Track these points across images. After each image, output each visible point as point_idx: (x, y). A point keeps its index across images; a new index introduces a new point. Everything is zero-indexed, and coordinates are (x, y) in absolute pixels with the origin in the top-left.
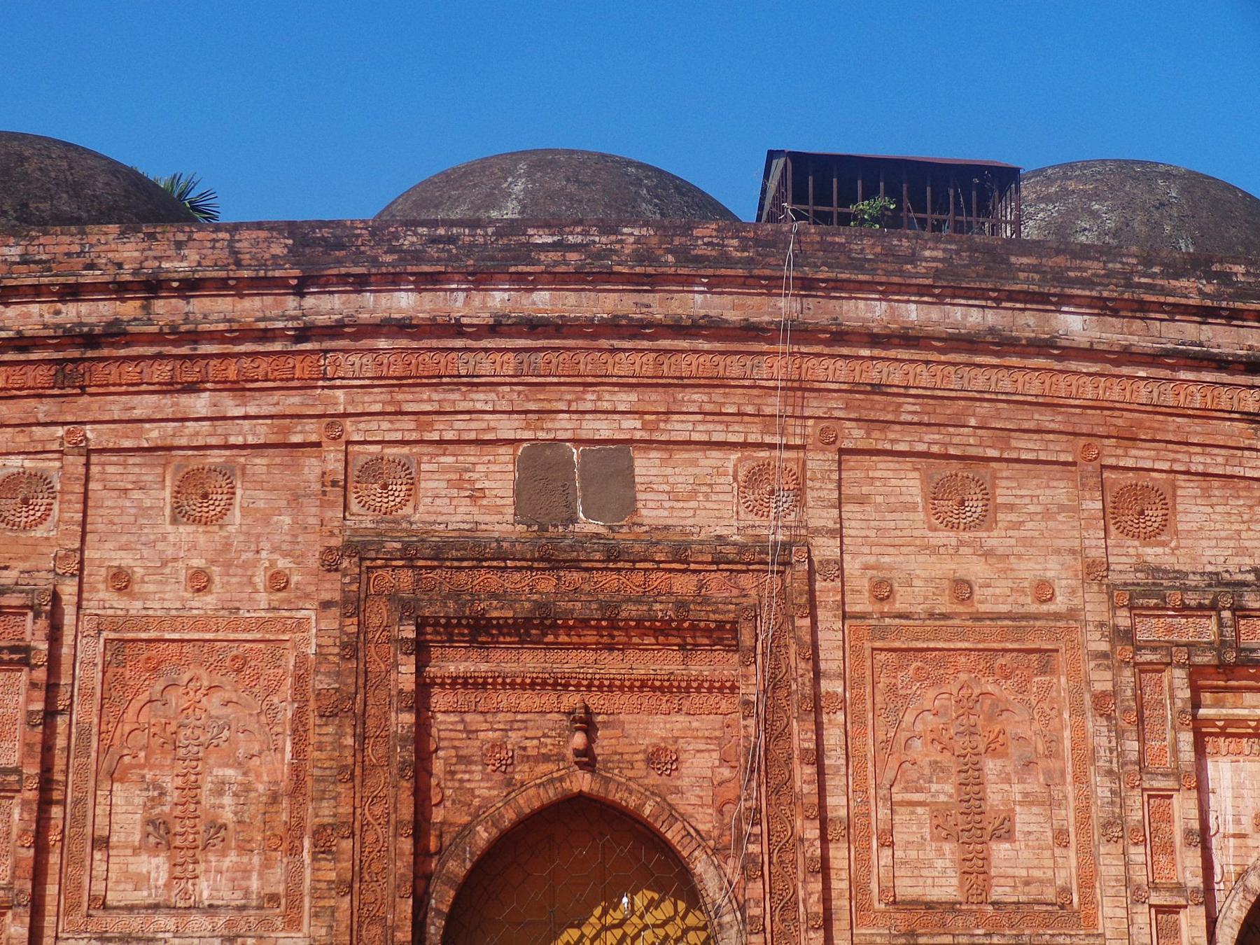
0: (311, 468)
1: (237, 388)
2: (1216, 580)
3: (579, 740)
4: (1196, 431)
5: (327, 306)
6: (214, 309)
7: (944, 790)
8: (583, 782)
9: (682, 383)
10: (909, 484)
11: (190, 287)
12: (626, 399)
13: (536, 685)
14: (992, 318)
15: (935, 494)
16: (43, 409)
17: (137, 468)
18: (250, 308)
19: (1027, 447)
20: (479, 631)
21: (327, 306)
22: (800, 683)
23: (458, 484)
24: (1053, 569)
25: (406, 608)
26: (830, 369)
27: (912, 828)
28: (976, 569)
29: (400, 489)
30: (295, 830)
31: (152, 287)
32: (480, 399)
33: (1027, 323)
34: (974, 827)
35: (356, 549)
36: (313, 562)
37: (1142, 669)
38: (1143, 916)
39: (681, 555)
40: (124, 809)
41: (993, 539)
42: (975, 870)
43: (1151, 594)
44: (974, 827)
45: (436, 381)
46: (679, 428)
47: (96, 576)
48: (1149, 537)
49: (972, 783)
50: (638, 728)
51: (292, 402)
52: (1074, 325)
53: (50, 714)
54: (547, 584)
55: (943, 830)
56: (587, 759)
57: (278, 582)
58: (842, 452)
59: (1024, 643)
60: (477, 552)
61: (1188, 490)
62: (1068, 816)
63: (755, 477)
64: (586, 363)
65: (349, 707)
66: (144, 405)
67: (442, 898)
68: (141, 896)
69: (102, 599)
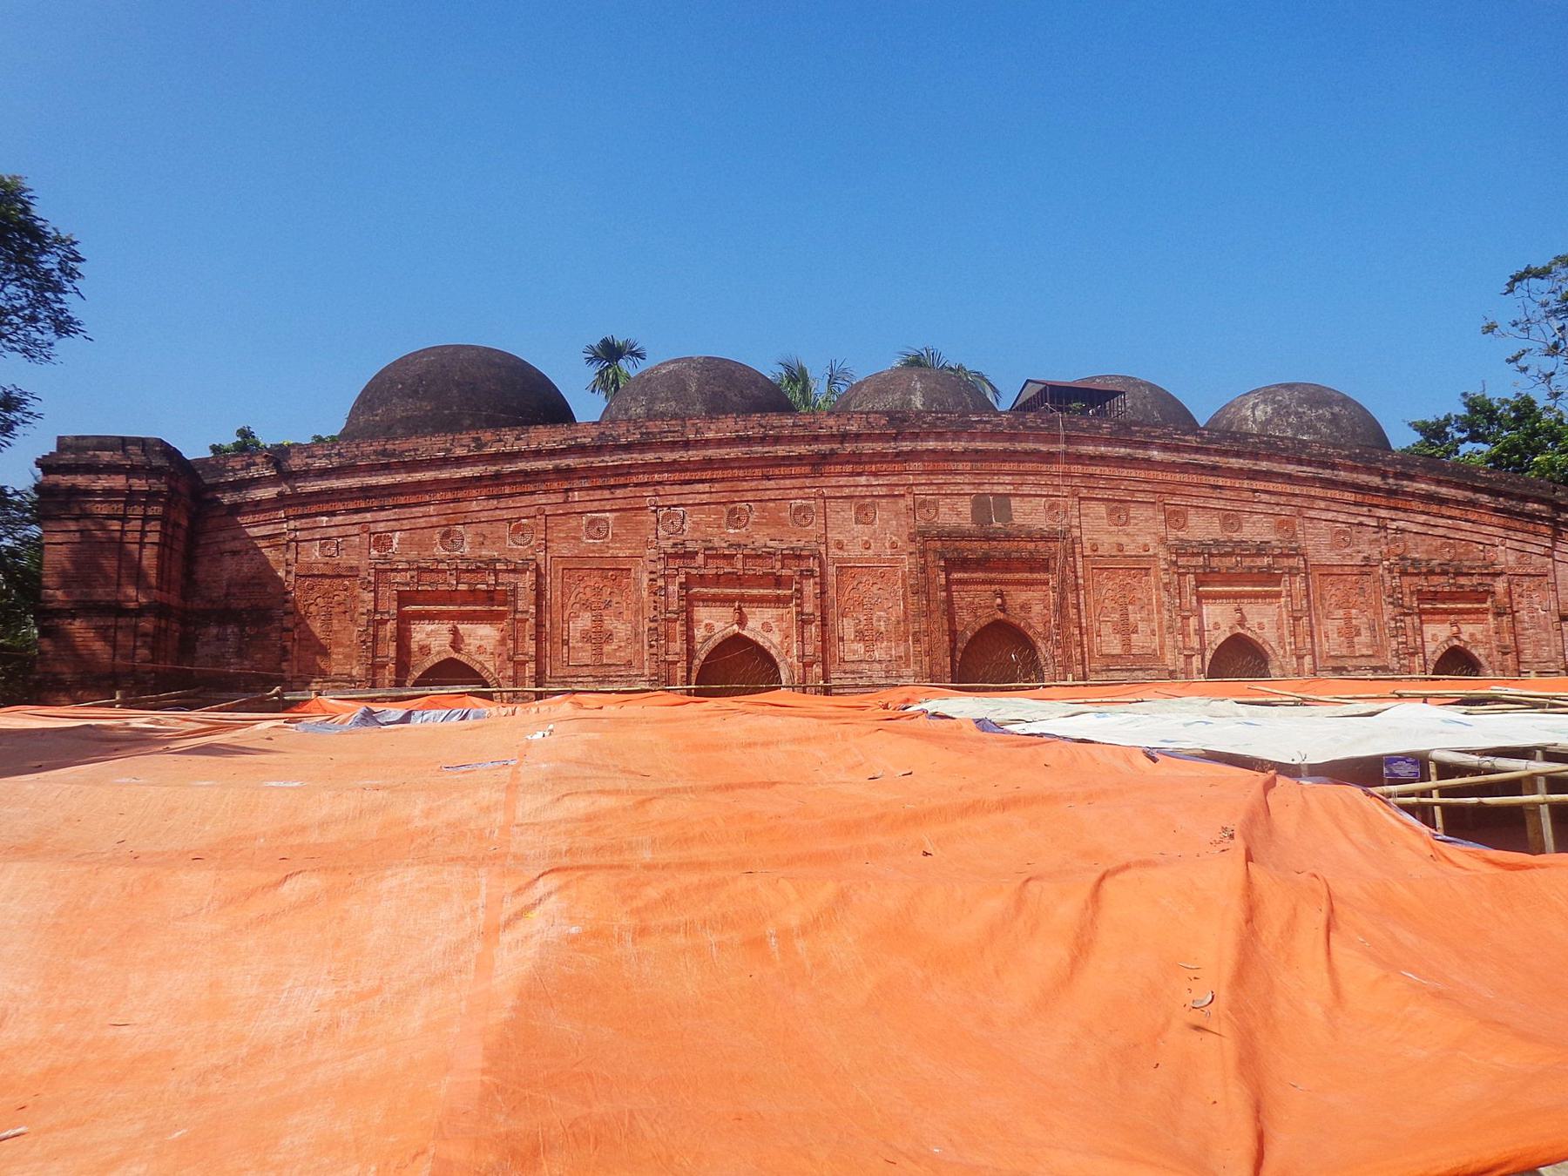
0: (902, 503)
1: (875, 474)
2: (1201, 543)
3: (999, 601)
4: (1194, 491)
5: (906, 446)
6: (867, 447)
7: (1116, 617)
8: (1001, 616)
9: (1027, 473)
10: (1102, 509)
11: (857, 437)
12: (1008, 479)
13: (984, 582)
14: (1123, 451)
15: (1110, 513)
16: (808, 482)
17: (845, 505)
18: (879, 446)
19: (1140, 497)
20: (963, 564)
21: (906, 446)
22: (1071, 580)
23: (952, 509)
24: (1148, 539)
25: (942, 557)
26: (1077, 469)
27: (1106, 629)
28: (1124, 540)
29: (933, 512)
30: (906, 633)
31: (844, 437)
32: (959, 479)
33: (1140, 453)
35: (922, 534)
36: (905, 537)
37: (1180, 574)
38: (1182, 658)
39: (1030, 537)
40: (847, 627)
41: (1129, 529)
42: (1127, 644)
43: (1181, 549)
44: (1126, 629)
45: (945, 472)
46: (1026, 490)
47: (832, 544)
48: (1179, 529)
49: (1125, 615)
50: (1019, 596)
51: (894, 480)
52: (1156, 455)
53: (823, 593)
54: (986, 546)
55: (1116, 631)
56: (1004, 611)
57: (894, 546)
58: (1081, 499)
59: (1139, 567)
60: (965, 536)
61: (1192, 511)
62: (1155, 625)
63: (1051, 507)
64: (995, 466)
65: (922, 589)
66: (843, 481)
67: (959, 656)
68: (856, 658)
69: (833, 551)
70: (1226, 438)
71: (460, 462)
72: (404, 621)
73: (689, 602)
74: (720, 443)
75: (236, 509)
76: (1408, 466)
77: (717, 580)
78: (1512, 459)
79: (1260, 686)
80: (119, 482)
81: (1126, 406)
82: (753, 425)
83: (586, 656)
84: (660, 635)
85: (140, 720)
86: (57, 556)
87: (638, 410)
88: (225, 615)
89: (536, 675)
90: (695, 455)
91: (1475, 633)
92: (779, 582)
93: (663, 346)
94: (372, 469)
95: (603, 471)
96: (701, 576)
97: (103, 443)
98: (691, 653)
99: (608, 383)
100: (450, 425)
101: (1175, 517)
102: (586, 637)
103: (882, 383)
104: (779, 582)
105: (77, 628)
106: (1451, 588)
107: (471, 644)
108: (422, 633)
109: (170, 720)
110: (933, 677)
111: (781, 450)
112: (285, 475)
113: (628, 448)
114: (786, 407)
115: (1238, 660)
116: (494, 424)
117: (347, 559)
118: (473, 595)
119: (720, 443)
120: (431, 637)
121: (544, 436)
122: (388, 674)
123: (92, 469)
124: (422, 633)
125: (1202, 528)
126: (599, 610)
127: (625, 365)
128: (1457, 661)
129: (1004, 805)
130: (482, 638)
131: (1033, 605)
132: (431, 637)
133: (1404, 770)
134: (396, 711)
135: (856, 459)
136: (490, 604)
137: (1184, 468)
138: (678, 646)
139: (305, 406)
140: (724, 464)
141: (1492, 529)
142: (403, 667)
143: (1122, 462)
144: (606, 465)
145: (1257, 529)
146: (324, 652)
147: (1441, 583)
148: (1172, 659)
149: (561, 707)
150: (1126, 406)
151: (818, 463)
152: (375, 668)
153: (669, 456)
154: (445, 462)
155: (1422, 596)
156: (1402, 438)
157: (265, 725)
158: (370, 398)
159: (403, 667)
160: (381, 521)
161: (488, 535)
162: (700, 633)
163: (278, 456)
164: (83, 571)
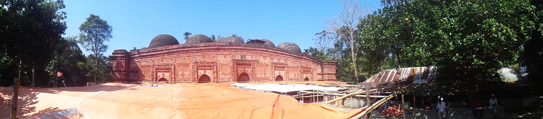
6: (226, 47)
10: (262, 57)
20: (239, 64)
31: (222, 46)
34: (265, 74)
40: (220, 73)
43: (273, 63)
44: (265, 74)
50: (247, 69)
70: (279, 49)
71: (164, 50)
72: (157, 72)
73: (198, 69)
74: (202, 47)
75: (133, 58)
76: (303, 55)
77: (202, 66)
78: (314, 55)
79: (281, 82)
80: (120, 55)
81: (267, 43)
82: (207, 44)
83: (181, 77)
84: (193, 74)
85: (124, 85)
86: (114, 65)
87: (190, 42)
88: (133, 72)
89: (174, 80)
90: (198, 48)
91: (309, 76)
92: (210, 66)
93: (195, 32)
94: (153, 52)
95: (186, 51)
96: (199, 66)
97: (119, 50)
98: (198, 77)
99: (187, 38)
100: (162, 45)
101: (272, 59)
102: (181, 75)
103: (229, 38)
104: (210, 66)
105: (116, 74)
106: (306, 70)
107: (165, 76)
108: (159, 74)
109: (127, 85)
110: (234, 81)
111: (211, 48)
112: (139, 53)
113: (189, 47)
114: (211, 42)
115: (279, 78)
116: (168, 45)
117: (149, 64)
118: (166, 69)
119: (202, 47)
120: (160, 75)
121: (175, 46)
122: (155, 80)
123: (117, 54)
124: (159, 74)
125: (276, 61)
126: (183, 71)
127: (189, 36)
128: (307, 79)
129: (241, 99)
130: (167, 75)
131: (249, 71)
132: (160, 75)
133: (299, 93)
134: (156, 85)
135: (224, 49)
136: (168, 70)
137: (273, 52)
138: (196, 76)
139: (143, 43)
140: (203, 50)
141: (311, 63)
142: (156, 79)
143: (265, 51)
144: (186, 50)
145: (282, 61)
146: (144, 77)
147: (306, 69)
148: (271, 78)
149: (179, 85)
150: (267, 43)
151: (219, 49)
152: (153, 79)
153: (195, 49)
154: (162, 51)
155: (303, 71)
156: (303, 51)
157: (138, 86)
158: (152, 43)
159: (156, 79)
160: (154, 59)
161: (168, 60)
162: (199, 74)
163: (138, 51)
164: (117, 66)
